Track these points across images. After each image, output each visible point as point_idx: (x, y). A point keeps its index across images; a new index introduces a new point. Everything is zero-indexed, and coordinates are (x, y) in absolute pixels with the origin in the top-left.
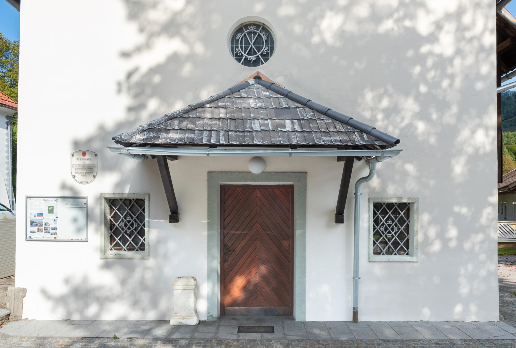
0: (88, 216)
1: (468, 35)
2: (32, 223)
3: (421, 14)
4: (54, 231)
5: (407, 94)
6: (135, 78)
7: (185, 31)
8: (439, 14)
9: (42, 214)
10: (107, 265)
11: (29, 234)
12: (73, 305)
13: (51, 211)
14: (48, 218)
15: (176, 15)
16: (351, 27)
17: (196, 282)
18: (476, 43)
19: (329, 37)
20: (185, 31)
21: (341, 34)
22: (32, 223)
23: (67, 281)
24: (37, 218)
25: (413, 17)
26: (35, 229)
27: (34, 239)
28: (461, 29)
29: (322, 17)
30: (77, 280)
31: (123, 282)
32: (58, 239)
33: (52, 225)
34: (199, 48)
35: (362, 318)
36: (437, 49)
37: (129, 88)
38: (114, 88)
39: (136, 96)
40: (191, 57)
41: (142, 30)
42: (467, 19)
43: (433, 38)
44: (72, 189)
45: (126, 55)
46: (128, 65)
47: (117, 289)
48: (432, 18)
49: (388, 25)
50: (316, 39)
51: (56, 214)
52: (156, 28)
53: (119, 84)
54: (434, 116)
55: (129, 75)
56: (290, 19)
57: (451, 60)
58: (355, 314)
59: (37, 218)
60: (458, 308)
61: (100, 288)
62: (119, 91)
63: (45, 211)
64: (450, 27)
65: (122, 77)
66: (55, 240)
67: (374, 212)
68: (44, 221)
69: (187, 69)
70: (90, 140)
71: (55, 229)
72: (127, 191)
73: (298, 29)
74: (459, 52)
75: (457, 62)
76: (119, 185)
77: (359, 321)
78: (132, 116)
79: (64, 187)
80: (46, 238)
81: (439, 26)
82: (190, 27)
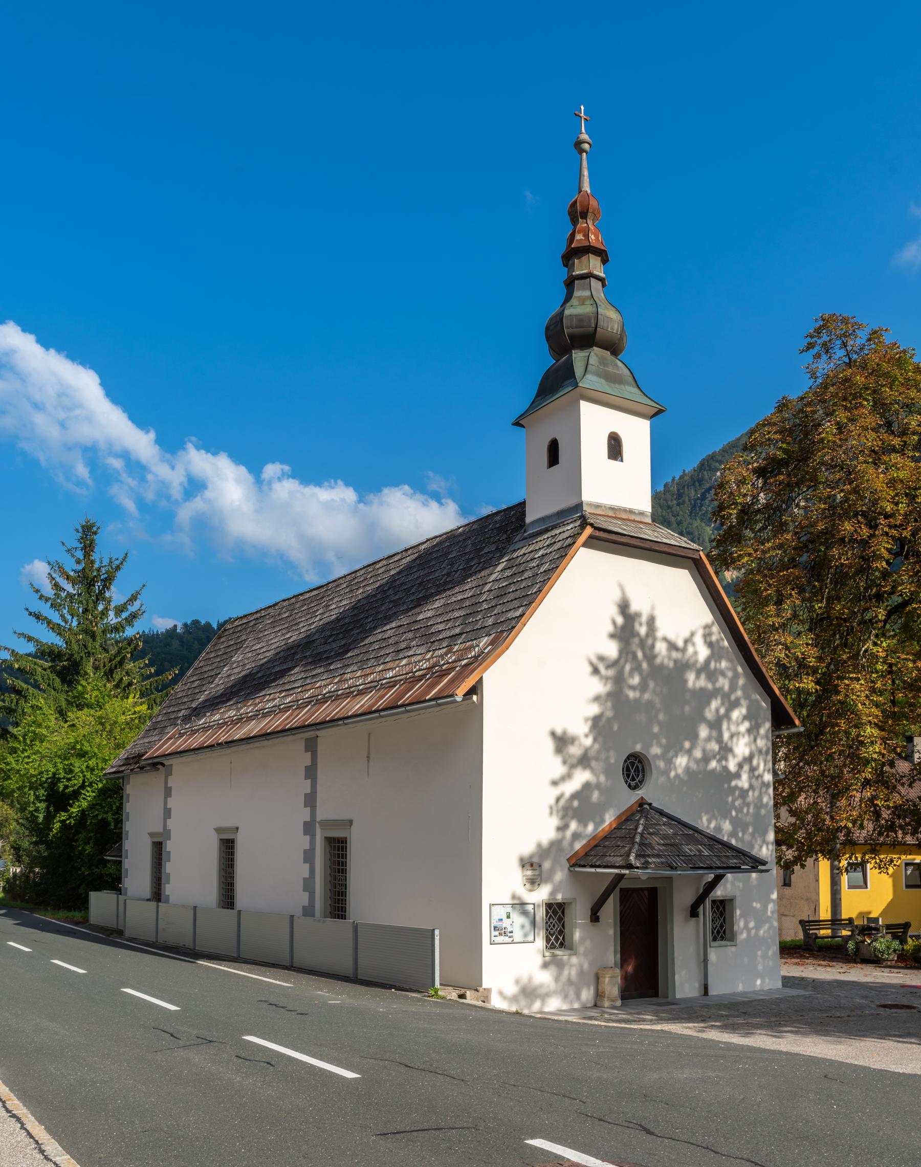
0: (534, 923)
1: (756, 773)
2: (495, 927)
3: (730, 758)
4: (511, 934)
5: (725, 818)
6: (562, 802)
7: (593, 763)
8: (740, 758)
9: (502, 920)
10: (545, 965)
11: (493, 938)
12: (523, 1002)
13: (508, 917)
14: (506, 923)
15: (587, 750)
16: (693, 766)
17: (779, 811)
18: (760, 780)
19: (680, 771)
20: (593, 763)
21: (687, 770)
22: (495, 927)
23: (517, 982)
24: (498, 923)
25: (726, 759)
26: (497, 933)
27: (496, 942)
28: (753, 770)
29: (677, 756)
30: (525, 980)
31: (557, 980)
32: (515, 941)
33: (510, 929)
34: (602, 778)
35: (713, 992)
36: (740, 784)
37: (558, 811)
38: (547, 811)
39: (563, 817)
40: (598, 786)
41: (564, 762)
42: (755, 762)
43: (738, 776)
44: (519, 899)
45: (555, 783)
46: (556, 792)
47: (553, 986)
48: (737, 760)
49: (713, 764)
50: (672, 774)
51: (513, 918)
52: (574, 761)
53: (551, 808)
54: (740, 834)
55: (558, 800)
56: (656, 757)
57: (747, 791)
58: (706, 990)
59: (498, 923)
60: (759, 982)
61: (541, 986)
62: (551, 813)
63: (504, 917)
64: (746, 768)
65: (552, 801)
66: (513, 942)
67: (712, 906)
68: (504, 926)
69: (595, 795)
70: (532, 856)
71: (511, 932)
72: (559, 897)
73: (662, 764)
74: (751, 787)
75: (750, 793)
76: (553, 893)
77: (709, 994)
78: (560, 835)
79: (514, 897)
80: (505, 942)
81: (740, 766)
82: (597, 759)
